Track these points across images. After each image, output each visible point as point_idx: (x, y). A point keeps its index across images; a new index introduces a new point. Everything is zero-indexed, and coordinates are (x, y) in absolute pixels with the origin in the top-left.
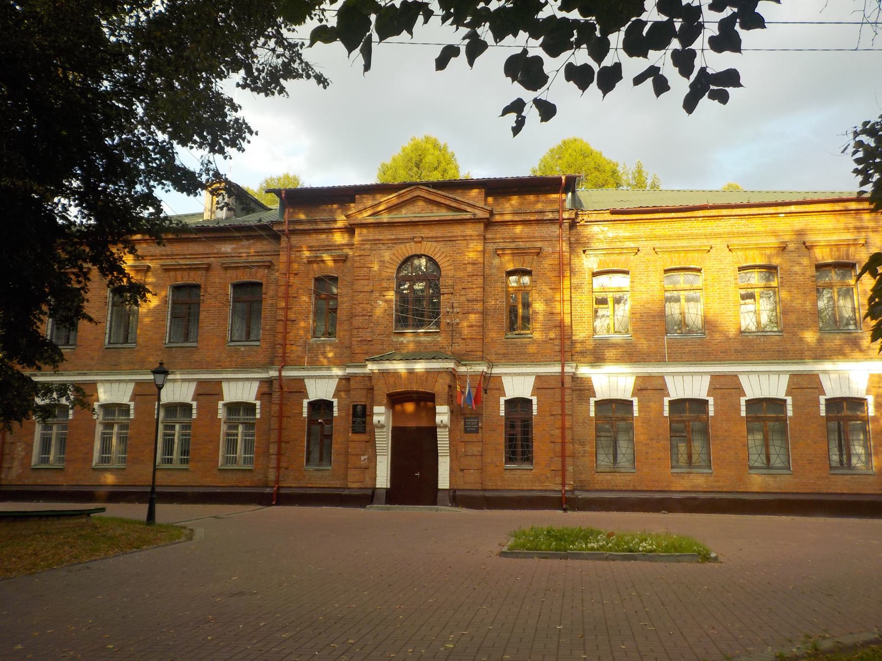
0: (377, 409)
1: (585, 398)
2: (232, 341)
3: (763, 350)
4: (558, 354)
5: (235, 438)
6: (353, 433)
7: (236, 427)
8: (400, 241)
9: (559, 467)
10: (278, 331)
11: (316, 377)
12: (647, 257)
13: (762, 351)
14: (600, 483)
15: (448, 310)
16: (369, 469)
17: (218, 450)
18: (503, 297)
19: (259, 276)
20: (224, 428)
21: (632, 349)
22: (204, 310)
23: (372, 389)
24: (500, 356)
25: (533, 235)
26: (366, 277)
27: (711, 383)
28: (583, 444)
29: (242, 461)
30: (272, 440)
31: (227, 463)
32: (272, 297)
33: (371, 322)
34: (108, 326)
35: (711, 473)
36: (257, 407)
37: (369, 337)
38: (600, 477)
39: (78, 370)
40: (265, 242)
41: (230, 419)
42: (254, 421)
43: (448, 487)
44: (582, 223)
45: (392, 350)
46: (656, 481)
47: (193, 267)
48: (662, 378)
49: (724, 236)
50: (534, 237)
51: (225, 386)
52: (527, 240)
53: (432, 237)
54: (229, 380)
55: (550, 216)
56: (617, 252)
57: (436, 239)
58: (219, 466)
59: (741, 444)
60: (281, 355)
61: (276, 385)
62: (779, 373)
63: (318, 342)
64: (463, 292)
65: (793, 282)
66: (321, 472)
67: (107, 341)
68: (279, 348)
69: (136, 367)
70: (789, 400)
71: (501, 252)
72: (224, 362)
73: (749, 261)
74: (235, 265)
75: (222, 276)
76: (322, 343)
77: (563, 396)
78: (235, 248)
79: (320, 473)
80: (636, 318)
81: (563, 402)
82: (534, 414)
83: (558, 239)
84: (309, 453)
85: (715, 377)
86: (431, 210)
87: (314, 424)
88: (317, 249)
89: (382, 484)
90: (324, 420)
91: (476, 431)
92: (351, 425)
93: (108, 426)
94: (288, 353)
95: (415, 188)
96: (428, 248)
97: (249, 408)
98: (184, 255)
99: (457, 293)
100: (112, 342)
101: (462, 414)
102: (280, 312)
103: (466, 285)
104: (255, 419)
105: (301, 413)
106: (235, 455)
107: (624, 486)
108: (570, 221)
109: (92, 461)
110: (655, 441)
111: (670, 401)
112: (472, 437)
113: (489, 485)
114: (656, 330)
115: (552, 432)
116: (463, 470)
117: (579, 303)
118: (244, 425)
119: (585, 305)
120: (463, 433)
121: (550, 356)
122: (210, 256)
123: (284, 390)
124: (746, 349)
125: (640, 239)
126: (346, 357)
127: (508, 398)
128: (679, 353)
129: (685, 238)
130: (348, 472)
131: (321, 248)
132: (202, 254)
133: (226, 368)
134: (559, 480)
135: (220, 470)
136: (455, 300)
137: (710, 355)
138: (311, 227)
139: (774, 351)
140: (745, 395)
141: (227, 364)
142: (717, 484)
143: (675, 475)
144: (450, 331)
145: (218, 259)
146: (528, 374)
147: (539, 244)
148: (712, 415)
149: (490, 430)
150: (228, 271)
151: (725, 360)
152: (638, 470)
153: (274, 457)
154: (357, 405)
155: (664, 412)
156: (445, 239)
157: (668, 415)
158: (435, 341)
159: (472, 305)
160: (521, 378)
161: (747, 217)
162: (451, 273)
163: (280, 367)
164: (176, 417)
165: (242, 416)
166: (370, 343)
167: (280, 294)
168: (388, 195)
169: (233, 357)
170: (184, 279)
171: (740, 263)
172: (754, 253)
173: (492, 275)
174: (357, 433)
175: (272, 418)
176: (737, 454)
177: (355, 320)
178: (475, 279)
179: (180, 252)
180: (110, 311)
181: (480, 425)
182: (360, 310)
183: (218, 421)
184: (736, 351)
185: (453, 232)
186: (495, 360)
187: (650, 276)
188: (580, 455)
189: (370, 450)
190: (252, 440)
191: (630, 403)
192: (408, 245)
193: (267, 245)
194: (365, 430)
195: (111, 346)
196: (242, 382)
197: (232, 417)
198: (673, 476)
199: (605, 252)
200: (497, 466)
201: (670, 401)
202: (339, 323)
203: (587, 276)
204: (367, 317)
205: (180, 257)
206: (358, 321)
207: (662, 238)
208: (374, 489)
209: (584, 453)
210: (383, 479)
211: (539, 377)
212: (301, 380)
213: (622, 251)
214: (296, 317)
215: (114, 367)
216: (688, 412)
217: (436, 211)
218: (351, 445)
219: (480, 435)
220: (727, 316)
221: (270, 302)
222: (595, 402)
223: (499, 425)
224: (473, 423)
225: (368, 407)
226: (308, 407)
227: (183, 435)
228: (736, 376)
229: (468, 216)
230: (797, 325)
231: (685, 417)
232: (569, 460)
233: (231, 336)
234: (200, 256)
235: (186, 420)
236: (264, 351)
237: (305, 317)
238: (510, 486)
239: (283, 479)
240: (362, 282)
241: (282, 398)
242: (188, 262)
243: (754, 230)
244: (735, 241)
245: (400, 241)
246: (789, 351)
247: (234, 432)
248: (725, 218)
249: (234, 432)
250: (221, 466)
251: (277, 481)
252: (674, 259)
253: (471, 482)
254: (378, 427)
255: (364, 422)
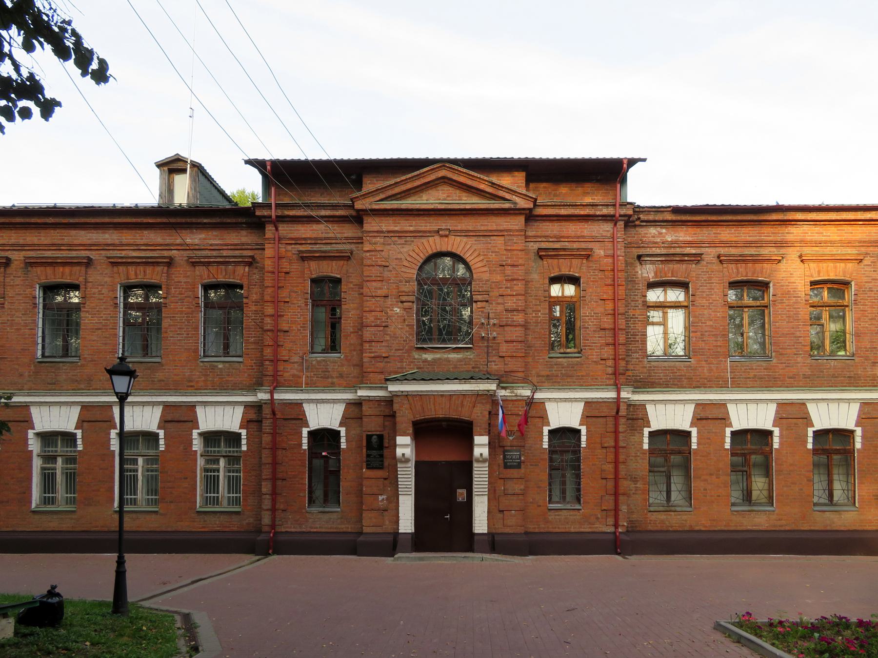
0: (400, 440)
1: (638, 429)
2: (205, 356)
3: (834, 376)
4: (611, 376)
5: (216, 474)
6: (367, 468)
7: (217, 461)
8: (420, 234)
9: (612, 506)
10: (266, 343)
11: (318, 401)
12: (709, 266)
13: (832, 377)
14: (653, 523)
15: (483, 321)
16: (389, 511)
17: (196, 489)
18: (546, 308)
19: (238, 275)
20: (200, 462)
21: (691, 373)
22: (167, 317)
23: (393, 416)
24: (544, 379)
25: (583, 234)
26: (379, 279)
27: (777, 412)
28: (635, 480)
29: (225, 502)
30: (264, 477)
31: (207, 504)
32: (256, 302)
33: (387, 335)
34: (40, 334)
35: (774, 511)
36: (242, 437)
37: (384, 352)
38: (653, 517)
39: (4, 389)
40: (244, 233)
41: (208, 451)
42: (239, 454)
43: (486, 532)
44: (637, 223)
45: (413, 369)
46: (714, 520)
47: (150, 260)
48: (725, 405)
49: (796, 245)
50: (583, 237)
51: (200, 411)
52: (575, 240)
53: (461, 231)
54: (205, 404)
55: (605, 211)
56: (677, 259)
57: (466, 234)
58: (198, 507)
59: (805, 479)
60: (272, 373)
61: (267, 411)
62: (849, 401)
63: (319, 359)
64: (500, 300)
65: (867, 299)
66: (328, 515)
67: (39, 353)
68: (268, 365)
69: (82, 386)
70: (161, 433)
71: (544, 253)
72: (197, 382)
73: (821, 274)
74: (206, 260)
75: (189, 273)
76: (324, 360)
77: (616, 425)
78: (205, 239)
79: (326, 516)
80: (696, 338)
81: (616, 432)
82: (582, 446)
83: (611, 240)
84: (311, 492)
85: (782, 405)
86: (459, 196)
87: (317, 458)
88: (313, 242)
89: (406, 528)
90: (328, 453)
91: (518, 466)
92: (365, 459)
93: (49, 459)
94: (281, 371)
95: (440, 167)
96: (456, 244)
97: (232, 438)
98: (137, 245)
99: (493, 300)
100: (47, 354)
101: (500, 447)
102: (268, 320)
103: (504, 291)
104: (240, 451)
105: (301, 445)
106: (216, 495)
107: (679, 527)
108: (626, 218)
109: (31, 503)
110: (714, 477)
111: (732, 432)
112: (514, 473)
113: (531, 528)
114: (717, 352)
115: (604, 467)
116: (503, 511)
117: (631, 318)
118: (227, 459)
119: (639, 321)
120: (502, 469)
121: (601, 379)
122: (172, 248)
123: (277, 417)
124: (815, 375)
125: (703, 245)
126: (354, 377)
127: (552, 428)
128: (743, 378)
129: (753, 245)
130: (364, 515)
131: (319, 242)
132: (161, 245)
133: (200, 389)
134: (611, 521)
135: (198, 512)
136: (491, 310)
137: (777, 381)
138: (306, 214)
139: (845, 377)
140: (813, 426)
141: (201, 384)
142: (779, 523)
143: (735, 513)
144: (486, 346)
145: (182, 252)
146: (576, 400)
147: (590, 245)
148: (777, 447)
149: (531, 465)
150: (197, 268)
151: (793, 387)
152: (695, 508)
153: (267, 496)
154: (372, 435)
155: (726, 444)
156: (478, 234)
157: (729, 447)
158: (467, 358)
159: (511, 315)
160: (568, 405)
161: (822, 223)
162: (485, 276)
163: (272, 388)
164: (138, 449)
165: (223, 449)
166: (386, 360)
167: (267, 298)
168: (404, 174)
169: (208, 375)
170: (140, 277)
171: (812, 276)
172: (828, 266)
173: (533, 282)
174: (373, 468)
175: (264, 451)
176: (802, 490)
177: (367, 331)
178: (515, 285)
179: (131, 241)
180: (41, 315)
181: (522, 458)
182: (372, 319)
183: (193, 453)
184: (805, 377)
185: (487, 225)
186: (538, 382)
187: (713, 289)
188: (632, 492)
189: (389, 489)
190: (237, 476)
191: (688, 434)
192: (430, 239)
193: (247, 236)
194: (383, 465)
195: (45, 360)
196: (222, 407)
197: (210, 449)
198: (734, 515)
199: (664, 259)
200: (540, 506)
201: (732, 432)
202: (344, 336)
203: (642, 286)
204: (382, 328)
205: (132, 248)
206: (368, 334)
207: (728, 245)
208: (396, 534)
209: (636, 490)
210: (407, 524)
211: (588, 404)
212: (299, 405)
213: (683, 259)
214: (290, 327)
215: (53, 386)
216: (749, 443)
217: (466, 198)
218: (365, 482)
219: (523, 470)
220: (795, 337)
221: (254, 308)
222: (650, 432)
223: (542, 459)
224: (514, 457)
225: (386, 436)
226: (308, 437)
227: (148, 471)
228: (804, 404)
229: (507, 205)
230: (869, 348)
231: (746, 449)
232: (621, 498)
233: (204, 350)
234: (158, 248)
235: (152, 452)
236: (249, 369)
237: (301, 327)
238: (555, 528)
239: (280, 522)
240: (374, 284)
241: (275, 426)
242: (142, 254)
243: (827, 238)
244: (807, 251)
245: (420, 234)
246: (860, 377)
247: (214, 466)
248: (798, 223)
249: (214, 466)
250: (200, 507)
251: (273, 526)
252: (740, 270)
253: (512, 524)
254: (401, 462)
255: (382, 456)
